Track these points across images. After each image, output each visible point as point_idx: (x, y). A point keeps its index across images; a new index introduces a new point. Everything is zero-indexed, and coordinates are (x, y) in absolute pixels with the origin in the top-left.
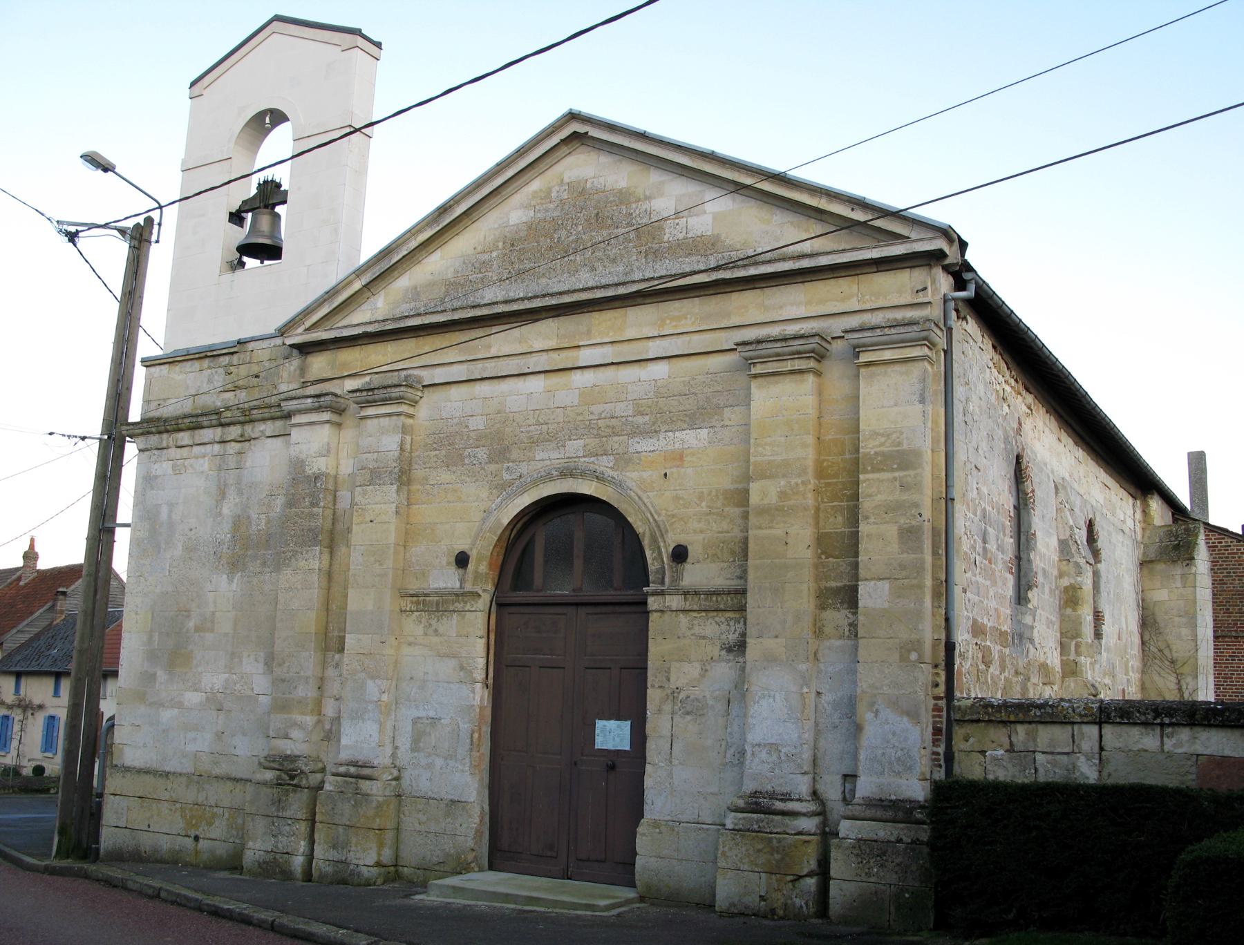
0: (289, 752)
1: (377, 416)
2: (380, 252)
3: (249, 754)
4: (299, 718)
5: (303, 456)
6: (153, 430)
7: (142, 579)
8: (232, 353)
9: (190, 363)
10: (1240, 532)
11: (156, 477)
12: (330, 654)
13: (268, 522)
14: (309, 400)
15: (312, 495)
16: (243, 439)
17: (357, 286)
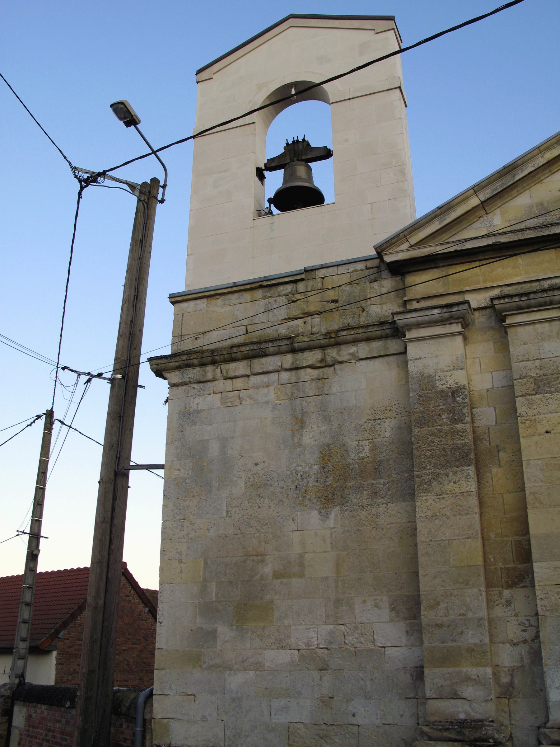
0: (462, 716)
1: (533, 323)
2: (504, 168)
3: (378, 722)
4: (473, 671)
5: (431, 371)
6: (195, 362)
7: (186, 523)
8: (295, 282)
9: (236, 295)
10: (38, 572)
11: (198, 412)
12: (496, 590)
13: (374, 448)
14: (436, 311)
15: (451, 411)
16: (324, 364)
17: (474, 202)
